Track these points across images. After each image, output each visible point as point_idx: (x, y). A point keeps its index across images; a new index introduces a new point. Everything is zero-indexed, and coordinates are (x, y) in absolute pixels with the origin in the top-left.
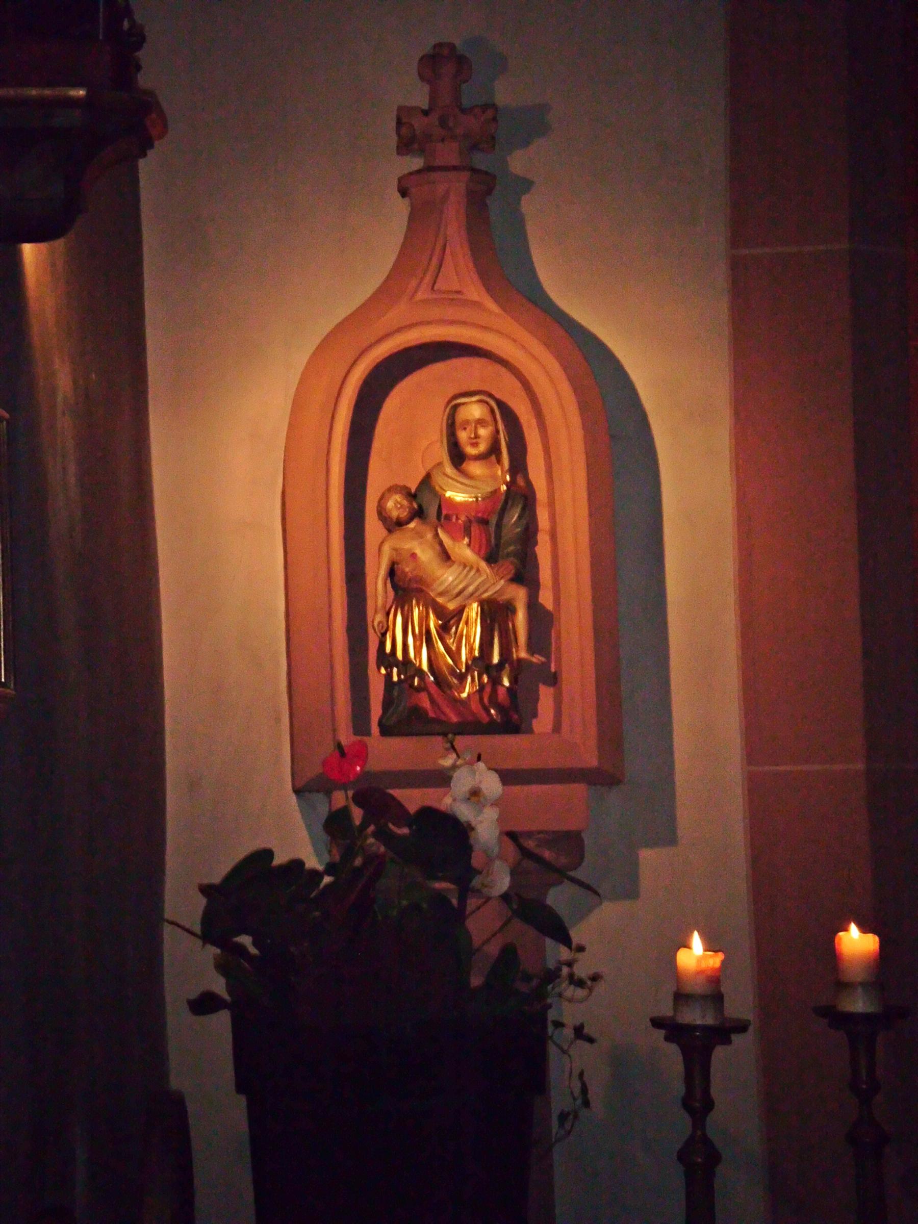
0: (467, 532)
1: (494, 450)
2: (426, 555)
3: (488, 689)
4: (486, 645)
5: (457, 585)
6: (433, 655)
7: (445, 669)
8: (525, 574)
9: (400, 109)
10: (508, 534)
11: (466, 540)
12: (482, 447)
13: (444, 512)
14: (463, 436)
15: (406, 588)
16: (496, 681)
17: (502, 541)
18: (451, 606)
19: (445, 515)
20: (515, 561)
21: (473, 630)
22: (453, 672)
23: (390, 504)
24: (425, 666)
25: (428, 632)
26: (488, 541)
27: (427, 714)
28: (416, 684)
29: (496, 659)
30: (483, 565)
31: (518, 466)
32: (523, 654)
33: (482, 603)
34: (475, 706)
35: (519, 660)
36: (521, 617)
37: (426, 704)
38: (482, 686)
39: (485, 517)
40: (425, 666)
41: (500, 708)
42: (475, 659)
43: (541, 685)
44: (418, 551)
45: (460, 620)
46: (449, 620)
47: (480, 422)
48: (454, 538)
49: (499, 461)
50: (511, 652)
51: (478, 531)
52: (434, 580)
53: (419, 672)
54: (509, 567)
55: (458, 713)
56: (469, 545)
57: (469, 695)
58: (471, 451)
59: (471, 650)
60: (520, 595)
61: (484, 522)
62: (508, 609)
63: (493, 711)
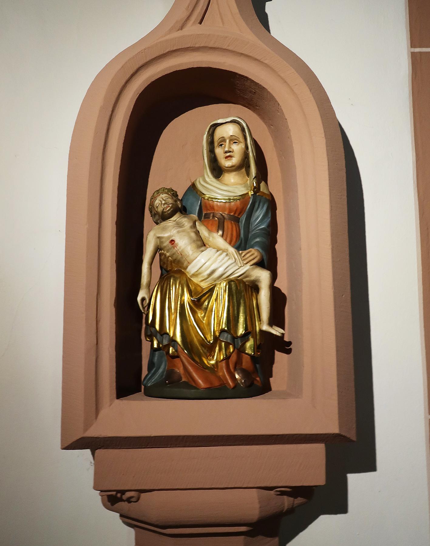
0: (221, 226)
1: (244, 165)
2: (184, 244)
3: (234, 358)
4: (232, 320)
5: (210, 266)
6: (185, 327)
7: (195, 339)
8: (269, 262)
9: (265, 388)
10: (256, 226)
11: (220, 233)
12: (235, 161)
13: (204, 213)
14: (219, 151)
15: (172, 269)
16: (241, 350)
17: (250, 235)
18: (205, 285)
19: (206, 213)
20: (260, 250)
21: (219, 307)
22: (203, 343)
23: (157, 202)
24: (179, 339)
25: (182, 306)
26: (239, 235)
27: (180, 378)
28: (170, 352)
29: (241, 331)
30: (232, 250)
31: (262, 174)
32: (265, 328)
33: (230, 282)
34: (223, 372)
35: (261, 331)
36: (264, 296)
37: (180, 370)
38: (227, 358)
39: (236, 215)
40: (179, 339)
41: (245, 373)
42: (222, 331)
43: (276, 353)
44: (178, 240)
45: (211, 295)
46: (200, 300)
47: (233, 140)
48: (210, 231)
49: (248, 173)
50: (253, 325)
51: (230, 226)
52: (189, 263)
53: (173, 341)
54: (254, 253)
55: (206, 380)
56: (222, 236)
57: (217, 362)
58: (227, 163)
59: (219, 324)
60: (263, 276)
61: (236, 220)
62: (255, 287)
63: (237, 376)
